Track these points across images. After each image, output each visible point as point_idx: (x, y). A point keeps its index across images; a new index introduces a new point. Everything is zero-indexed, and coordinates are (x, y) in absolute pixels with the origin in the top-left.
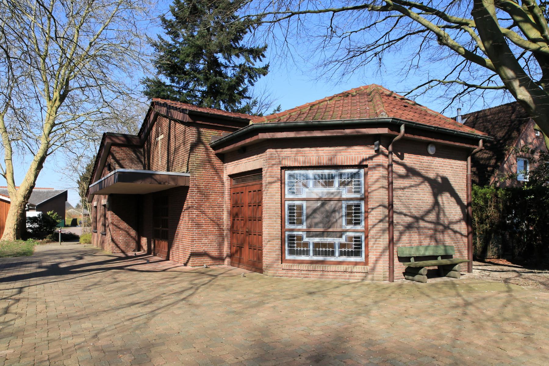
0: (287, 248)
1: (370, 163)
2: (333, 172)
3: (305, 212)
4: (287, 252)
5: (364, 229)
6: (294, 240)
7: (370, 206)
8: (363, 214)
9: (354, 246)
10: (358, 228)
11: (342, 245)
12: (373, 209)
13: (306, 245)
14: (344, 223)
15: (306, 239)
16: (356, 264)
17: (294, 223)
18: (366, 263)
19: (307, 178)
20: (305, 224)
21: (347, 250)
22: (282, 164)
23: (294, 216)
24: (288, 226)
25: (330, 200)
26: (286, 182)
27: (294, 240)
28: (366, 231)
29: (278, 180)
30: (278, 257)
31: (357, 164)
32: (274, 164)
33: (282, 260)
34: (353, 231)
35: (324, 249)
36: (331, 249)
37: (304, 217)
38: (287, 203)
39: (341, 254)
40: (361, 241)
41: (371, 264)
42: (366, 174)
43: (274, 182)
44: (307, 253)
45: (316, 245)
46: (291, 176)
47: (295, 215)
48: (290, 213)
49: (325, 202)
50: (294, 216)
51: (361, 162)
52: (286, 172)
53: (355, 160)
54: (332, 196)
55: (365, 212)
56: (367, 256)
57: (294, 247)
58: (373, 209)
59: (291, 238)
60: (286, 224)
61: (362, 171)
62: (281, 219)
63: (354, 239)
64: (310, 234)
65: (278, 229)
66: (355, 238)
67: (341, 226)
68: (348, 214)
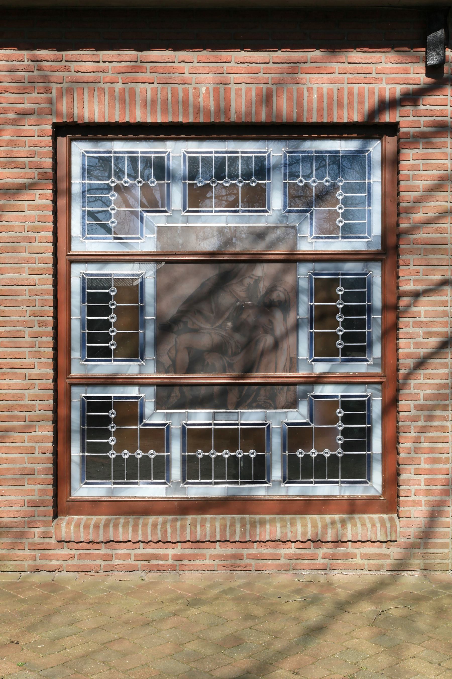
0: (76, 451)
1: (409, 120)
2: (275, 151)
3: (150, 312)
4: (76, 471)
5: (378, 371)
6: (107, 421)
7: (408, 285)
8: (377, 317)
9: (340, 440)
10: (359, 368)
11: (295, 437)
12: (417, 295)
13: (158, 437)
14: (304, 351)
15: (155, 417)
16: (353, 507)
17: (106, 353)
18: (390, 501)
19: (161, 169)
20: (150, 355)
21: (313, 453)
22: (59, 114)
23: (107, 325)
24: (79, 365)
25: (254, 260)
26: (76, 188)
27: (107, 421)
28: (393, 387)
29: (43, 176)
30: (43, 493)
31: (356, 118)
32: (25, 114)
33: (55, 505)
34: (339, 379)
35: (226, 454)
36: (253, 454)
37: (150, 333)
38: (78, 272)
39: (295, 470)
40: (368, 419)
41: (414, 513)
42: (392, 163)
43: (23, 188)
44: (157, 470)
45: (195, 438)
46: (100, 166)
47: (112, 318)
48: (91, 311)
49: (226, 266)
50: (107, 325)
51: (373, 114)
52: (75, 144)
53: (351, 103)
54: (259, 247)
55: (385, 307)
56: (392, 481)
57: (107, 447)
58: (417, 295)
59: (97, 415)
60: (76, 355)
61: (375, 149)
62: (56, 338)
63: (340, 413)
64: (170, 395)
65: (41, 377)
66: (346, 405)
67: (293, 363)
68: (321, 317)
